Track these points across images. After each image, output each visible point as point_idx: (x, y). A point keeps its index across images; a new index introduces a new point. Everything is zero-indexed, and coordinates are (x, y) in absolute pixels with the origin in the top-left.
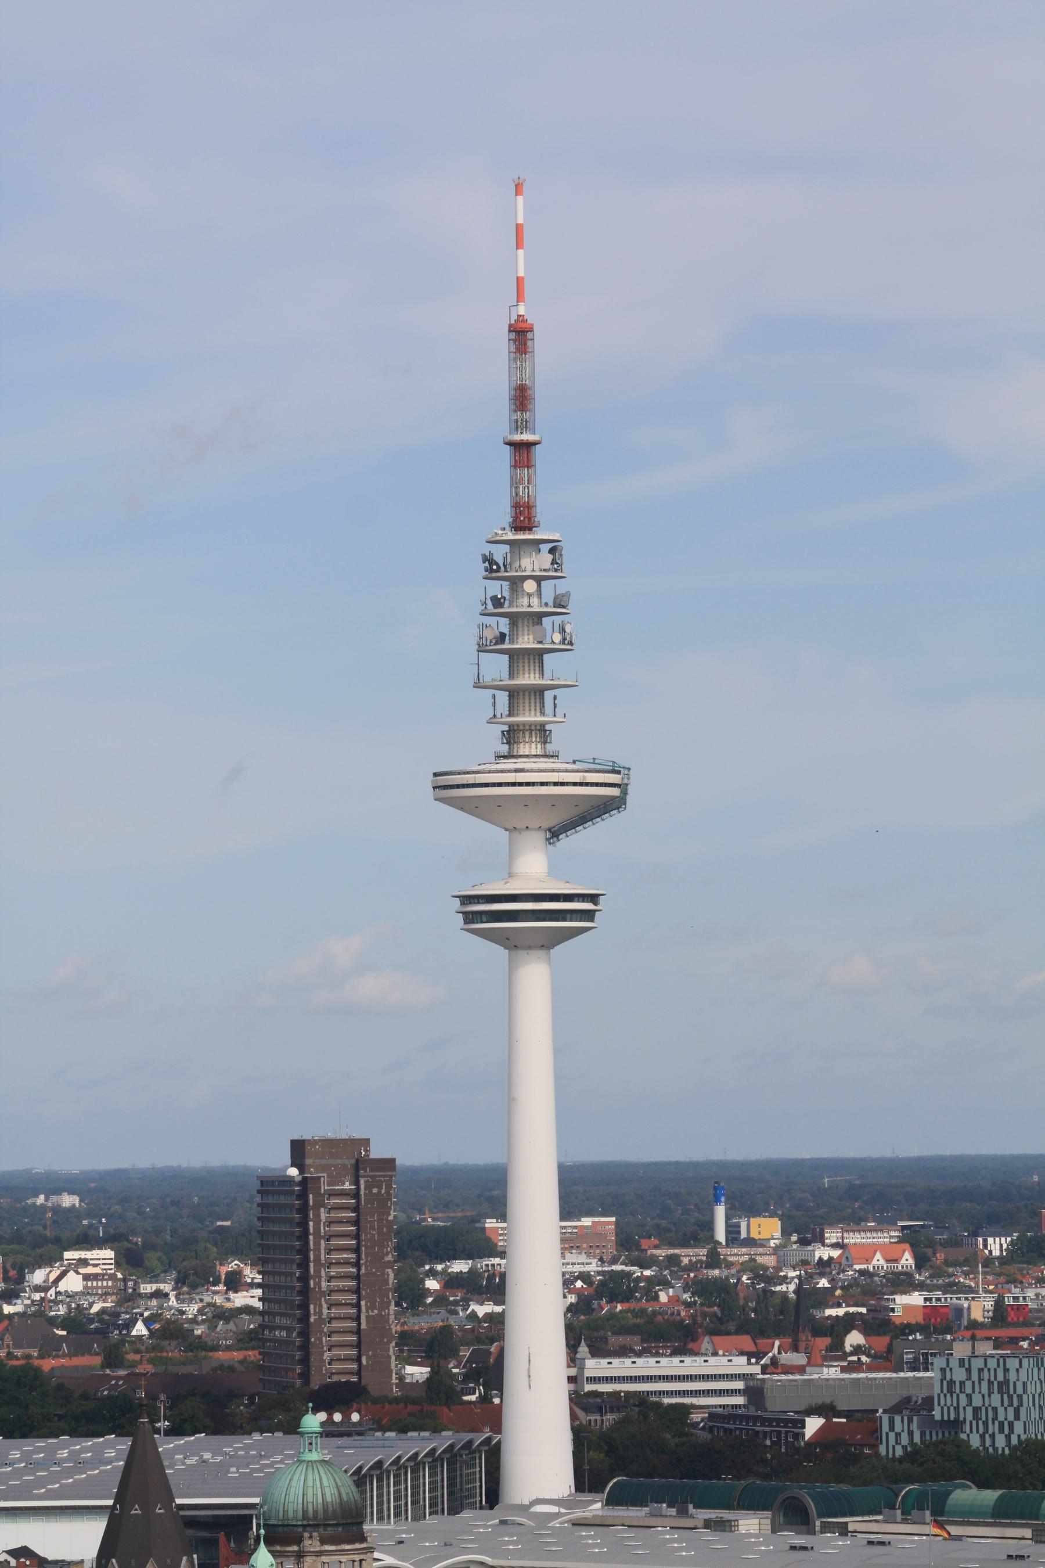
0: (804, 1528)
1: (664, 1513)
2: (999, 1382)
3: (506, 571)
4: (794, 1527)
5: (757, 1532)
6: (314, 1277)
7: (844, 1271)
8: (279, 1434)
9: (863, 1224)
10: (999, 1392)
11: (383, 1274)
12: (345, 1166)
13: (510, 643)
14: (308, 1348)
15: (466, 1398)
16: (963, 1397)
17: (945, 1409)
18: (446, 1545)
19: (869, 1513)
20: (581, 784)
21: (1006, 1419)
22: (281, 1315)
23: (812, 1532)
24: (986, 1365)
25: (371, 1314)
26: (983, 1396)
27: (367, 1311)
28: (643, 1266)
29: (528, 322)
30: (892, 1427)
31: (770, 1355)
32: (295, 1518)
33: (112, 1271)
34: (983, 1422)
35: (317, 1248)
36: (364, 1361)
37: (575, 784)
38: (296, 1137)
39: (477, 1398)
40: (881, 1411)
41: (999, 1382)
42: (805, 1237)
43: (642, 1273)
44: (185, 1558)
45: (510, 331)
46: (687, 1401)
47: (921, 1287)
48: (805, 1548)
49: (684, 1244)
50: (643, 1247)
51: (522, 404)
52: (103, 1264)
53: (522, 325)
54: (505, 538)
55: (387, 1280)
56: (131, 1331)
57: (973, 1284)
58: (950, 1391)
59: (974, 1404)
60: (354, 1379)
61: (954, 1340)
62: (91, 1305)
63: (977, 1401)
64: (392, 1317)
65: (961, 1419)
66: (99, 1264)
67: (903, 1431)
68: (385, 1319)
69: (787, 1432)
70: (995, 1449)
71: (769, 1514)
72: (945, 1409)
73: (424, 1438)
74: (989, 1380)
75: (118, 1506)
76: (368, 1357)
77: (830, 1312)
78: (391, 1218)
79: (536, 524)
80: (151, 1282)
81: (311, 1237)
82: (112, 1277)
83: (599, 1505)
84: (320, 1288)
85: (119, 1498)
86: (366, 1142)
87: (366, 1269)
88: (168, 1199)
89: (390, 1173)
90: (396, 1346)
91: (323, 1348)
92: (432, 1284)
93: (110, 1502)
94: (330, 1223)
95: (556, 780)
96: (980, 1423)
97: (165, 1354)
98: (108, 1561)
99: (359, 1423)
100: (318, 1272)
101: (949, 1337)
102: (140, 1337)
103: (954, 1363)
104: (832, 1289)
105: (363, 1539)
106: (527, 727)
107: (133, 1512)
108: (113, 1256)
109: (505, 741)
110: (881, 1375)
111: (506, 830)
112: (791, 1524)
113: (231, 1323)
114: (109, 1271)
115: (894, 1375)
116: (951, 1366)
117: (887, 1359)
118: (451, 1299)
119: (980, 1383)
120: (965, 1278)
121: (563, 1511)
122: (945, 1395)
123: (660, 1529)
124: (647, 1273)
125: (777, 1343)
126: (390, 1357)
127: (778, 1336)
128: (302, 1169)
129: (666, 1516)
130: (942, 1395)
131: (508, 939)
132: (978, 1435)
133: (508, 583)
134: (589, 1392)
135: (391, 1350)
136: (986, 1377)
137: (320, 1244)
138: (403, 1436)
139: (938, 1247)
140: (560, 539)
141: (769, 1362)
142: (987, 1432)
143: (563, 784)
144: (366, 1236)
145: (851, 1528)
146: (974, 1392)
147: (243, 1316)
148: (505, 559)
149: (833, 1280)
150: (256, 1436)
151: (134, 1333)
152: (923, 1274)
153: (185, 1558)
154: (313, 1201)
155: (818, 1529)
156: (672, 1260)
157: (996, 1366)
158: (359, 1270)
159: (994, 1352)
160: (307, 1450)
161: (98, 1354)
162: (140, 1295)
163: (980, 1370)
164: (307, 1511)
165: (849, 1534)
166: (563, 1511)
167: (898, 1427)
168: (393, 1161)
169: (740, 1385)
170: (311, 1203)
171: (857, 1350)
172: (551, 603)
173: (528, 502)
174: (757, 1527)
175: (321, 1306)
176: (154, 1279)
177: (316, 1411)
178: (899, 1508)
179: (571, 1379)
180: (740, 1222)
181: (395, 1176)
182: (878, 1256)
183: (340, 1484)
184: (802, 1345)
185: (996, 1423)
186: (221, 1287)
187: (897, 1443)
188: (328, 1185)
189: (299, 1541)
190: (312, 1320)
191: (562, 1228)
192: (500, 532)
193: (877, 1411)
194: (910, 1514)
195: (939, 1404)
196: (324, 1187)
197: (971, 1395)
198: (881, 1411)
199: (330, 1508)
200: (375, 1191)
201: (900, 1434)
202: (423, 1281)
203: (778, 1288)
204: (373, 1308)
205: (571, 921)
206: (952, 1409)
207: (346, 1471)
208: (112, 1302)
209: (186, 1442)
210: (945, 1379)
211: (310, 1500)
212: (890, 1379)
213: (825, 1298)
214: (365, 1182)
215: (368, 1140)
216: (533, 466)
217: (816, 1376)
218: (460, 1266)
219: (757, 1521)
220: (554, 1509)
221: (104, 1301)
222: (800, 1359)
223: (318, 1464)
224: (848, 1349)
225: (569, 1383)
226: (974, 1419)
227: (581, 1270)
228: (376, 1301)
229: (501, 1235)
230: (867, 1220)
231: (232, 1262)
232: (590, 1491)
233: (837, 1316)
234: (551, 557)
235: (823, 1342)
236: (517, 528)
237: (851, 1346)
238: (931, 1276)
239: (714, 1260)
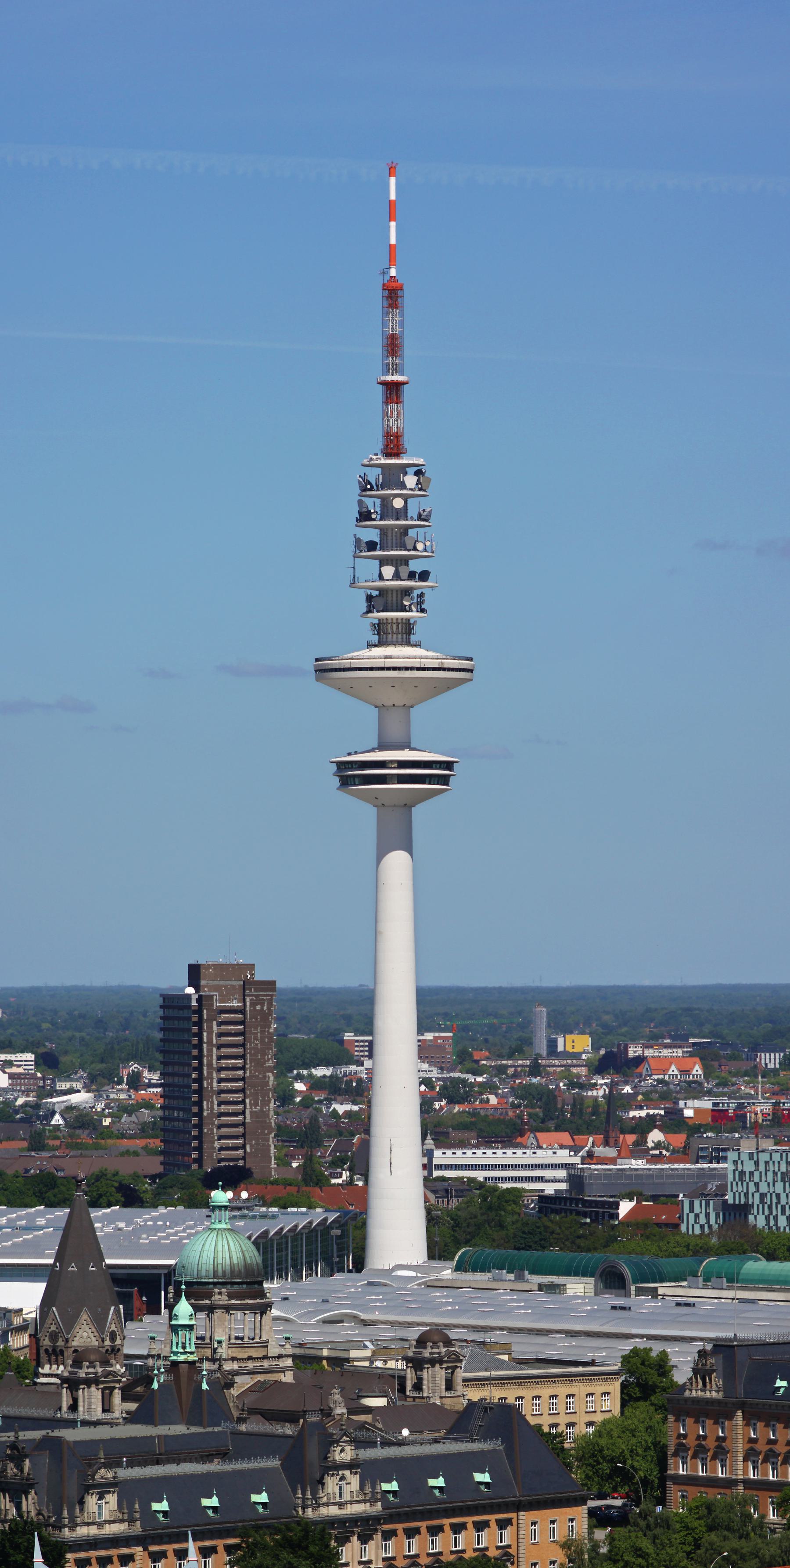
0: (623, 1291)
1: (503, 1278)
2: (782, 1173)
3: (378, 490)
4: (614, 1291)
5: (582, 1294)
6: (207, 1079)
7: (645, 1080)
8: (180, 1208)
9: (660, 1041)
10: (781, 1181)
11: (265, 1077)
12: (233, 986)
13: (380, 550)
14: (202, 1137)
15: (333, 1181)
16: (751, 1185)
17: (737, 1194)
18: (323, 1301)
19: (676, 1280)
20: (439, 669)
21: (787, 1203)
22: (179, 1109)
23: (627, 1295)
24: (771, 1159)
25: (254, 1110)
26: (769, 1184)
27: (251, 1108)
28: (476, 1073)
29: (399, 282)
30: (692, 1209)
31: (587, 1148)
32: (207, 1276)
33: (33, 1072)
34: (769, 1206)
35: (210, 1055)
36: (248, 1150)
37: (434, 669)
38: (193, 962)
39: (343, 1181)
40: (681, 1195)
41: (782, 1173)
42: (611, 1051)
43: (475, 1079)
44: (113, 1308)
45: (384, 289)
46: (518, 1185)
47: (709, 1093)
48: (623, 1308)
49: (510, 1056)
50: (475, 1058)
51: (393, 350)
52: (25, 1065)
53: (394, 285)
54: (379, 462)
55: (268, 1082)
56: (51, 1121)
57: (753, 1093)
58: (741, 1180)
59: (761, 1191)
60: (241, 1163)
61: (741, 1138)
62: (16, 1099)
63: (763, 1188)
64: (272, 1113)
65: (750, 1203)
66: (22, 1065)
67: (701, 1212)
68: (265, 1114)
69: (604, 1212)
70: (778, 1228)
71: (591, 1280)
72: (737, 1194)
73: (303, 1214)
74: (774, 1171)
75: (58, 1264)
76: (251, 1146)
77: (632, 1114)
78: (272, 1030)
79: (403, 450)
80: (65, 1081)
81: (205, 1046)
82: (33, 1077)
83: (449, 1271)
84: (212, 1088)
85: (59, 1257)
86: (251, 967)
87: (251, 1072)
88: (76, 1013)
89: (271, 993)
90: (275, 1137)
91: (214, 1137)
92: (300, 1086)
93: (51, 1261)
94: (220, 1035)
95: (418, 666)
96: (766, 1206)
97: (80, 1141)
98: (50, 1308)
99: (247, 1200)
100: (210, 1073)
101: (737, 1135)
102: (57, 1127)
103: (745, 1157)
104: (636, 1094)
105: (262, 1295)
106: (400, 621)
107: (70, 1269)
108: (33, 1058)
109: (376, 632)
110: (681, 1166)
111: (376, 707)
112: (610, 1288)
113: (133, 1115)
114: (30, 1071)
115: (692, 1166)
116: (742, 1159)
117: (683, 1154)
118: (316, 1099)
119: (766, 1174)
120: (746, 1087)
121: (419, 1275)
122: (737, 1184)
123: (502, 1291)
124: (480, 1079)
125: (591, 1139)
126: (270, 1146)
127: (590, 1133)
128: (197, 989)
129: (506, 1281)
130: (734, 1183)
131: (376, 798)
132: (764, 1216)
133: (380, 500)
134: (437, 1177)
135: (271, 1140)
136: (772, 1168)
137: (212, 1051)
138: (282, 1210)
139: (723, 1061)
140: (424, 463)
141: (585, 1154)
142: (772, 1214)
143: (424, 669)
144: (250, 1045)
145: (660, 1292)
146: (761, 1180)
147: (143, 1110)
148: (377, 479)
149: (635, 1087)
150: (162, 1210)
151: (53, 1123)
152: (710, 1083)
153: (113, 1308)
154: (207, 1015)
155: (633, 1293)
156: (501, 1070)
157: (779, 1160)
158: (245, 1073)
159: (775, 1148)
160: (217, 1221)
161: (24, 1139)
162: (56, 1091)
163: (767, 1163)
164: (217, 1271)
165: (660, 1297)
166: (419, 1275)
167: (697, 1209)
168: (273, 983)
169: (562, 1174)
170: (205, 1017)
171: (658, 1146)
172: (415, 517)
173: (397, 432)
174: (582, 1290)
175: (213, 1103)
176: (68, 1078)
177: (224, 1189)
178: (701, 1276)
179: (424, 1167)
180: (557, 1039)
181: (275, 996)
182: (673, 1067)
183: (244, 1249)
184: (612, 1141)
185: (779, 1206)
186: (124, 1086)
187: (695, 1222)
188: (220, 1002)
189: (209, 1296)
190: (205, 1114)
191: (419, 1041)
192: (374, 457)
193: (678, 1196)
194: (710, 1281)
195: (732, 1190)
196: (217, 1004)
197: (758, 1183)
198: (681, 1195)
199: (236, 1269)
200: (258, 1007)
201: (698, 1215)
202: (292, 1084)
203: (590, 1093)
204: (256, 1105)
205: (430, 784)
206: (742, 1194)
207: (249, 1238)
208: (33, 1097)
209: (103, 1214)
210: (737, 1170)
211: (220, 1261)
212: (689, 1169)
213: (629, 1102)
214: (250, 1000)
215: (253, 965)
216: (401, 402)
217: (627, 1167)
218: (320, 1072)
219: (582, 1285)
220: (412, 1274)
221: (28, 1096)
222: (611, 1152)
223: (227, 1232)
224: (650, 1144)
225: (423, 1169)
226: (760, 1203)
227: (424, 1076)
228: (259, 1099)
229: (357, 1046)
230: (664, 1038)
231: (133, 1065)
232: (440, 1259)
233: (640, 1117)
234: (416, 478)
235: (631, 1138)
236: (388, 454)
237: (653, 1141)
238: (717, 1085)
239: (535, 1069)
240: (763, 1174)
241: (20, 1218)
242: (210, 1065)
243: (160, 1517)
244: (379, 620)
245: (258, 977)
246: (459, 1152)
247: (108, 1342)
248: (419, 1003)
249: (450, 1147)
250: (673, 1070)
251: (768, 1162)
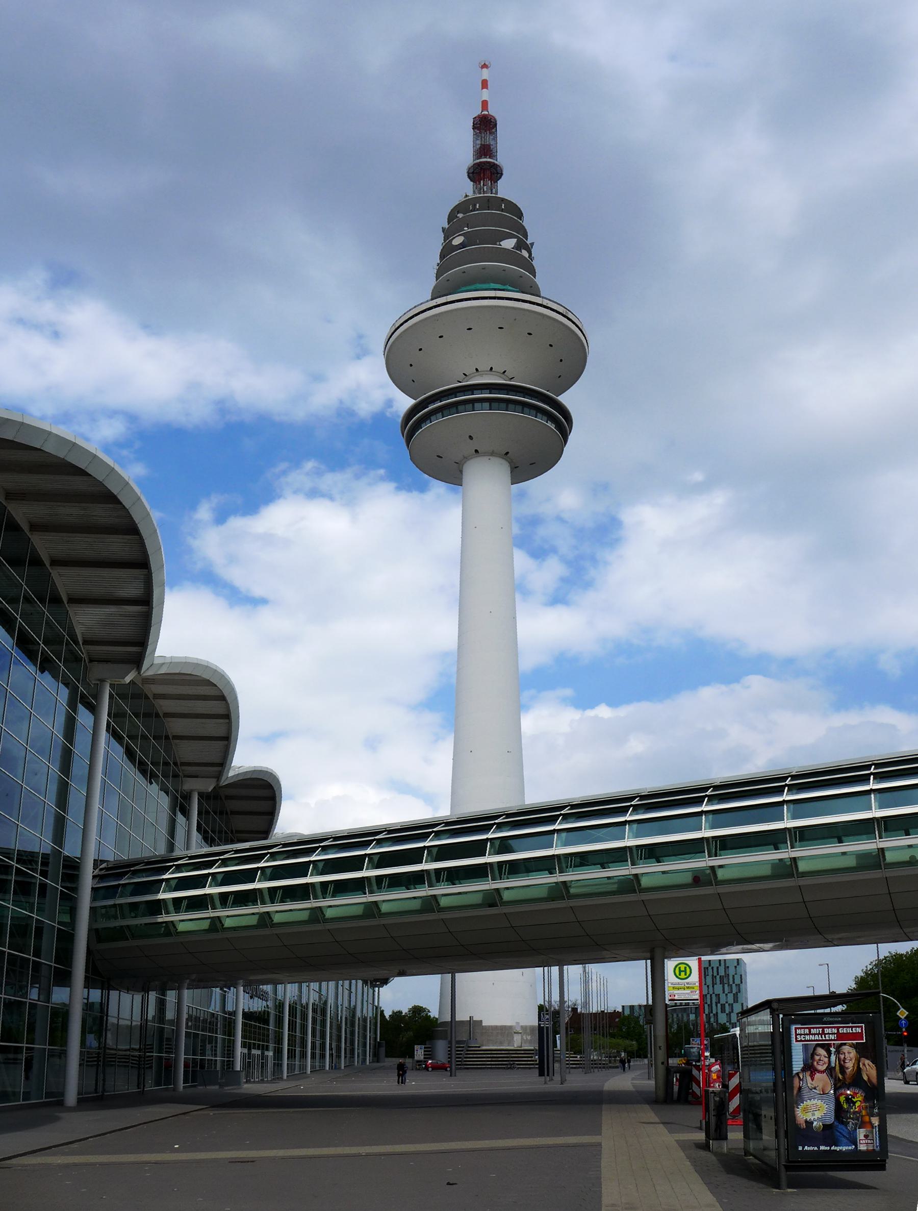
26: (708, 986)
86: (443, 229)
136: (710, 973)
185: (719, 1005)
240: (711, 987)
244: (85, 988)
251: (707, 968)
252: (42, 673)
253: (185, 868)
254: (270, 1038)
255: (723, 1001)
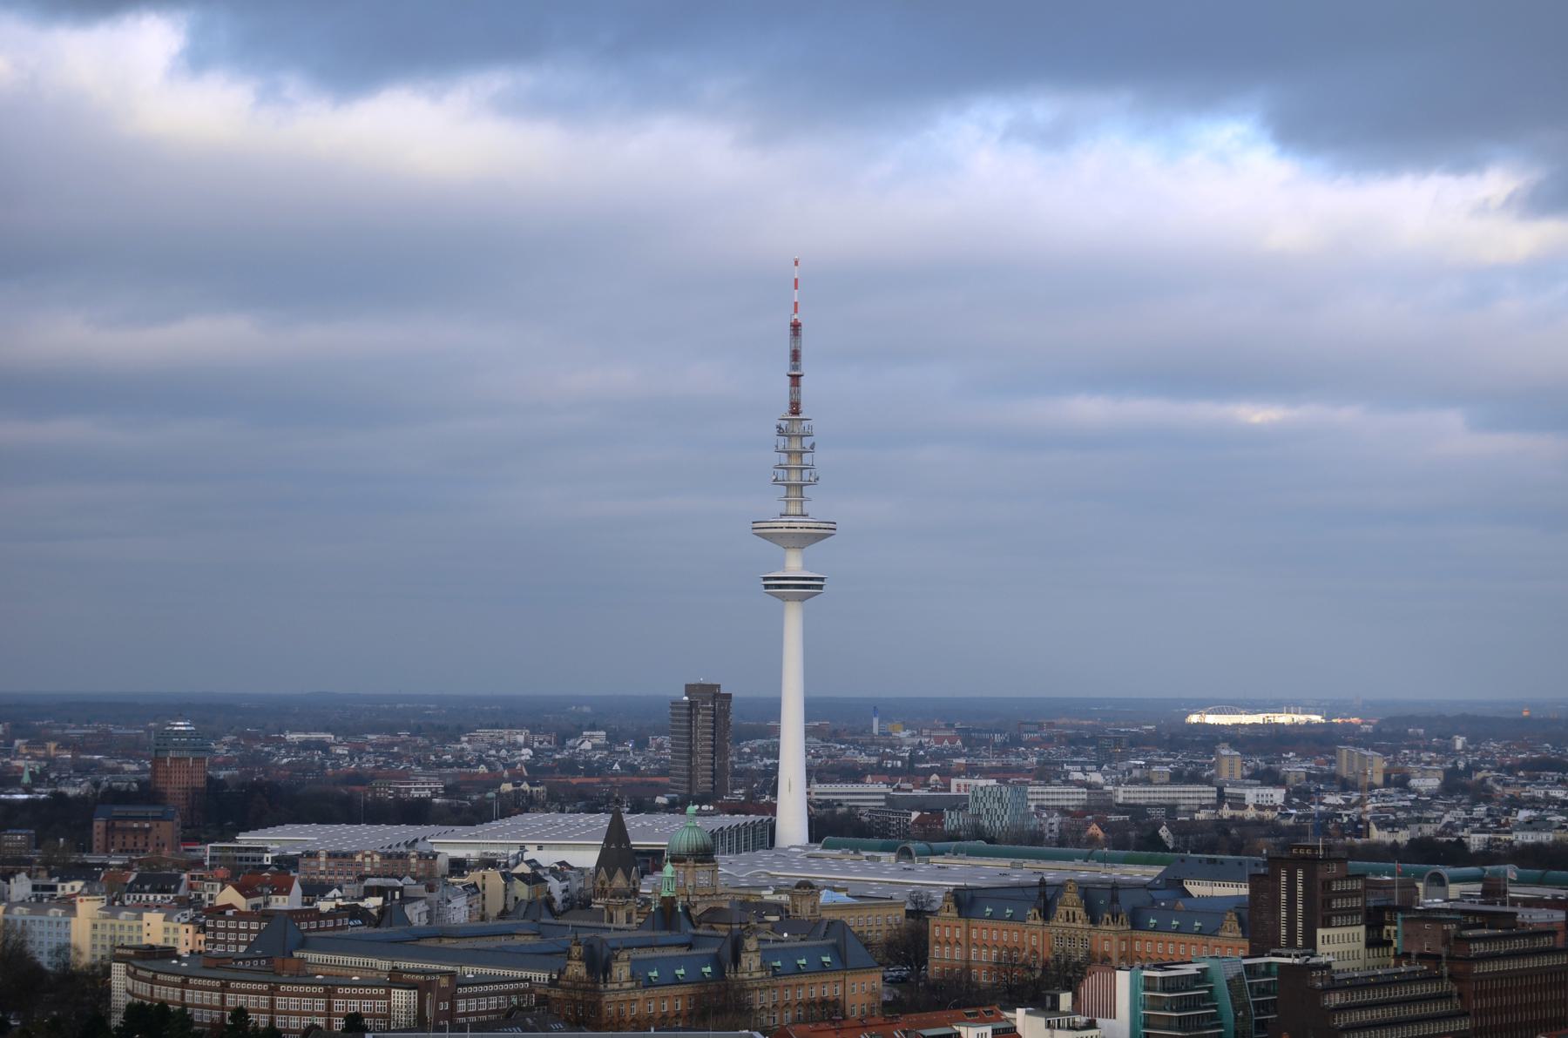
30: (950, 817)
47: (964, 755)
63: (988, 806)
86: (719, 686)
100: (696, 744)
105: (714, 861)
163: (990, 792)
182: (946, 741)
220: (799, 850)
222: (909, 786)
241: (570, 819)
242: (696, 737)
243: (679, 977)
245: (722, 692)
246: (828, 786)
247: (632, 886)
248: (805, 705)
249: (824, 783)
250: (946, 743)
252: (687, 686)
253: (1393, 904)
254: (611, 900)
255: (998, 813)
